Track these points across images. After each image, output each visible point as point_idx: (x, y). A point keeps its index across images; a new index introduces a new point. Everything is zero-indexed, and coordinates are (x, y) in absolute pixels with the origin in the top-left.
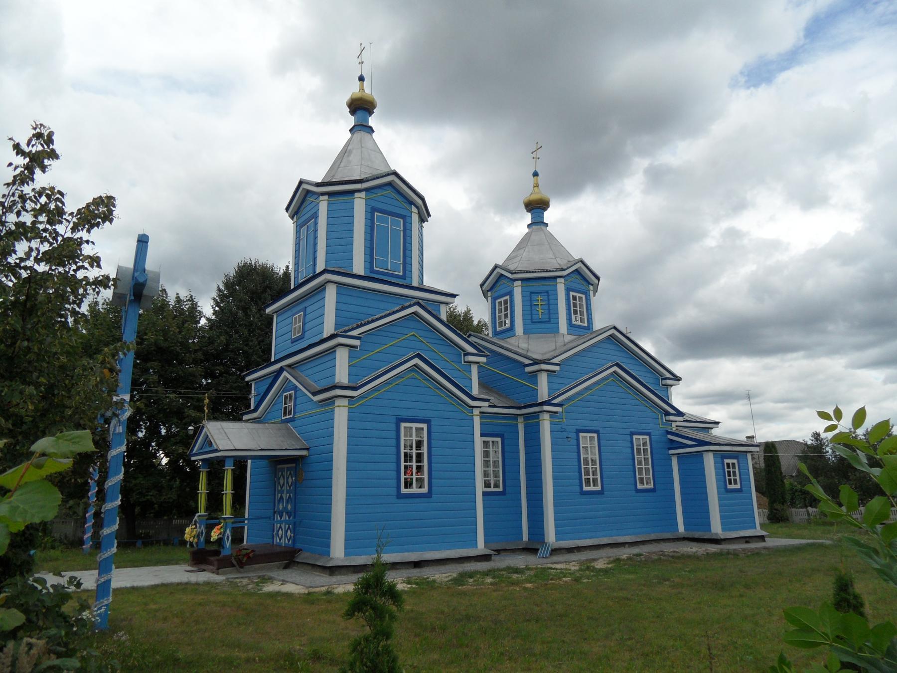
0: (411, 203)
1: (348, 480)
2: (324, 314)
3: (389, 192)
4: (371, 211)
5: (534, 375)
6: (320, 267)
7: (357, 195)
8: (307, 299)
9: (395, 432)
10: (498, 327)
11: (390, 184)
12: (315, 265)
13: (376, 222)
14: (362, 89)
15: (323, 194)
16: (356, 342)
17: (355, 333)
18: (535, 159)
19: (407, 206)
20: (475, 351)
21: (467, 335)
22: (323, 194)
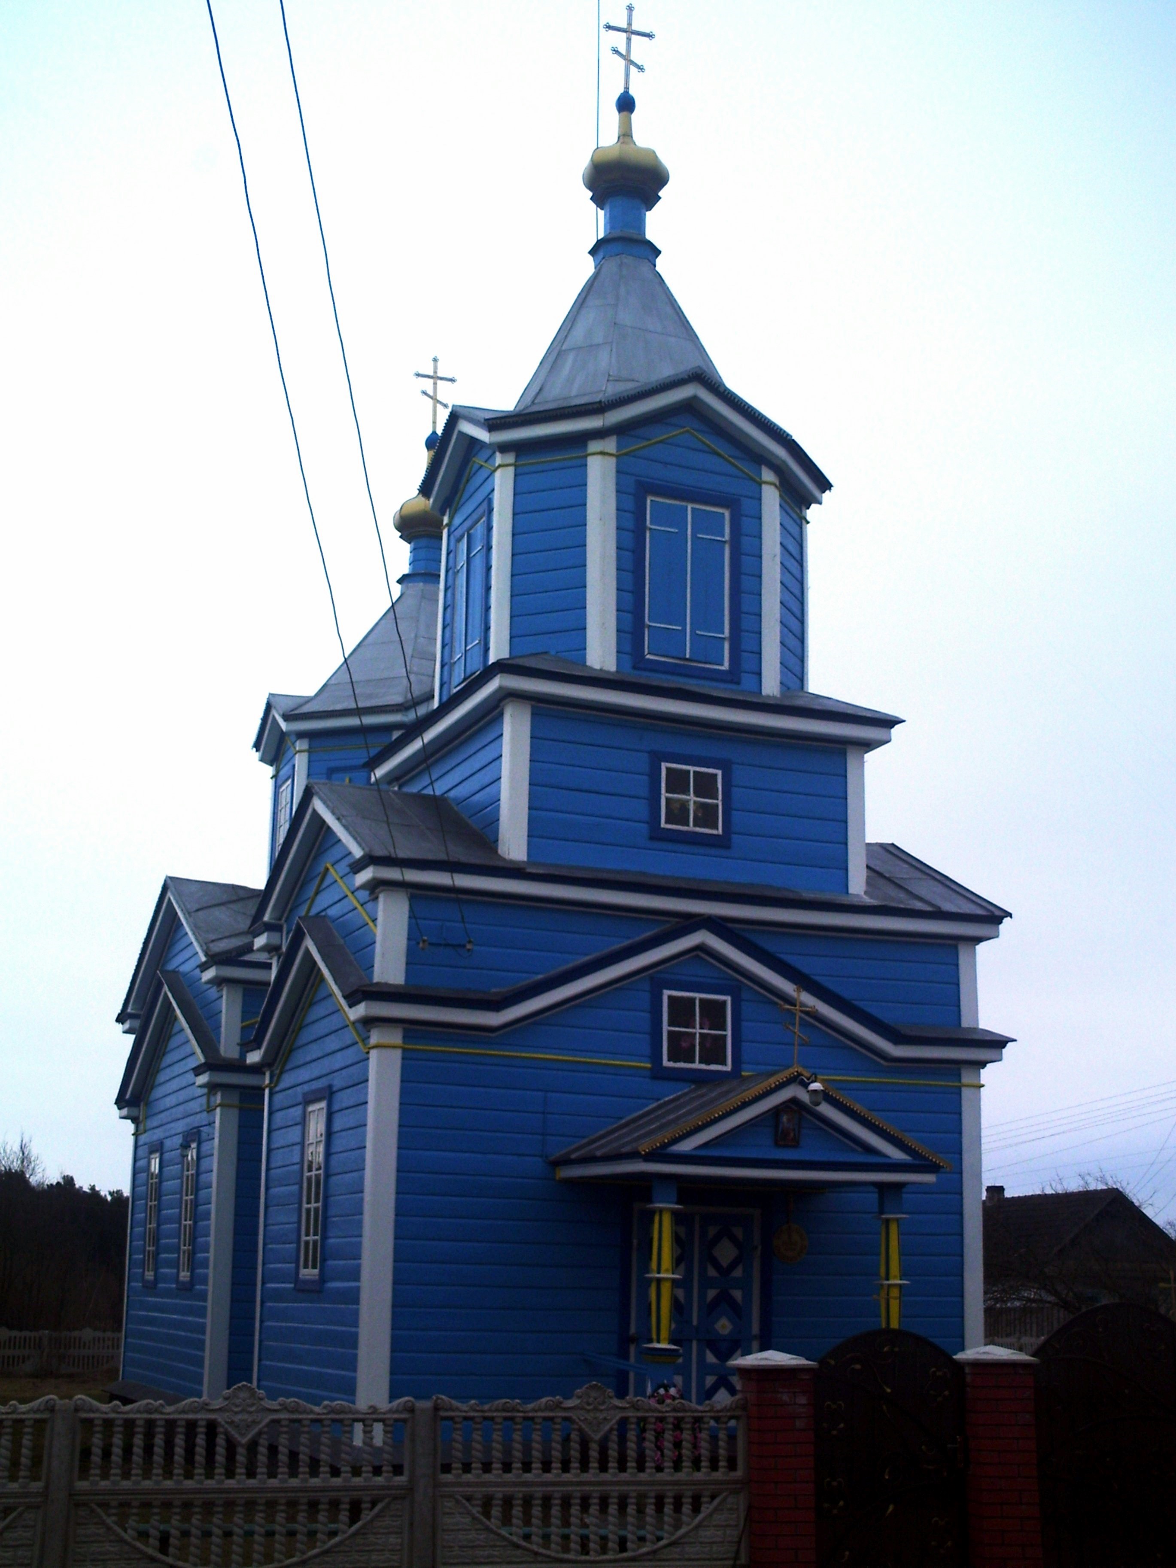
0: (761, 458)
2: (501, 756)
6: (498, 650)
9: (645, 826)
11: (690, 407)
12: (487, 649)
13: (651, 523)
14: (626, 134)
19: (746, 467)
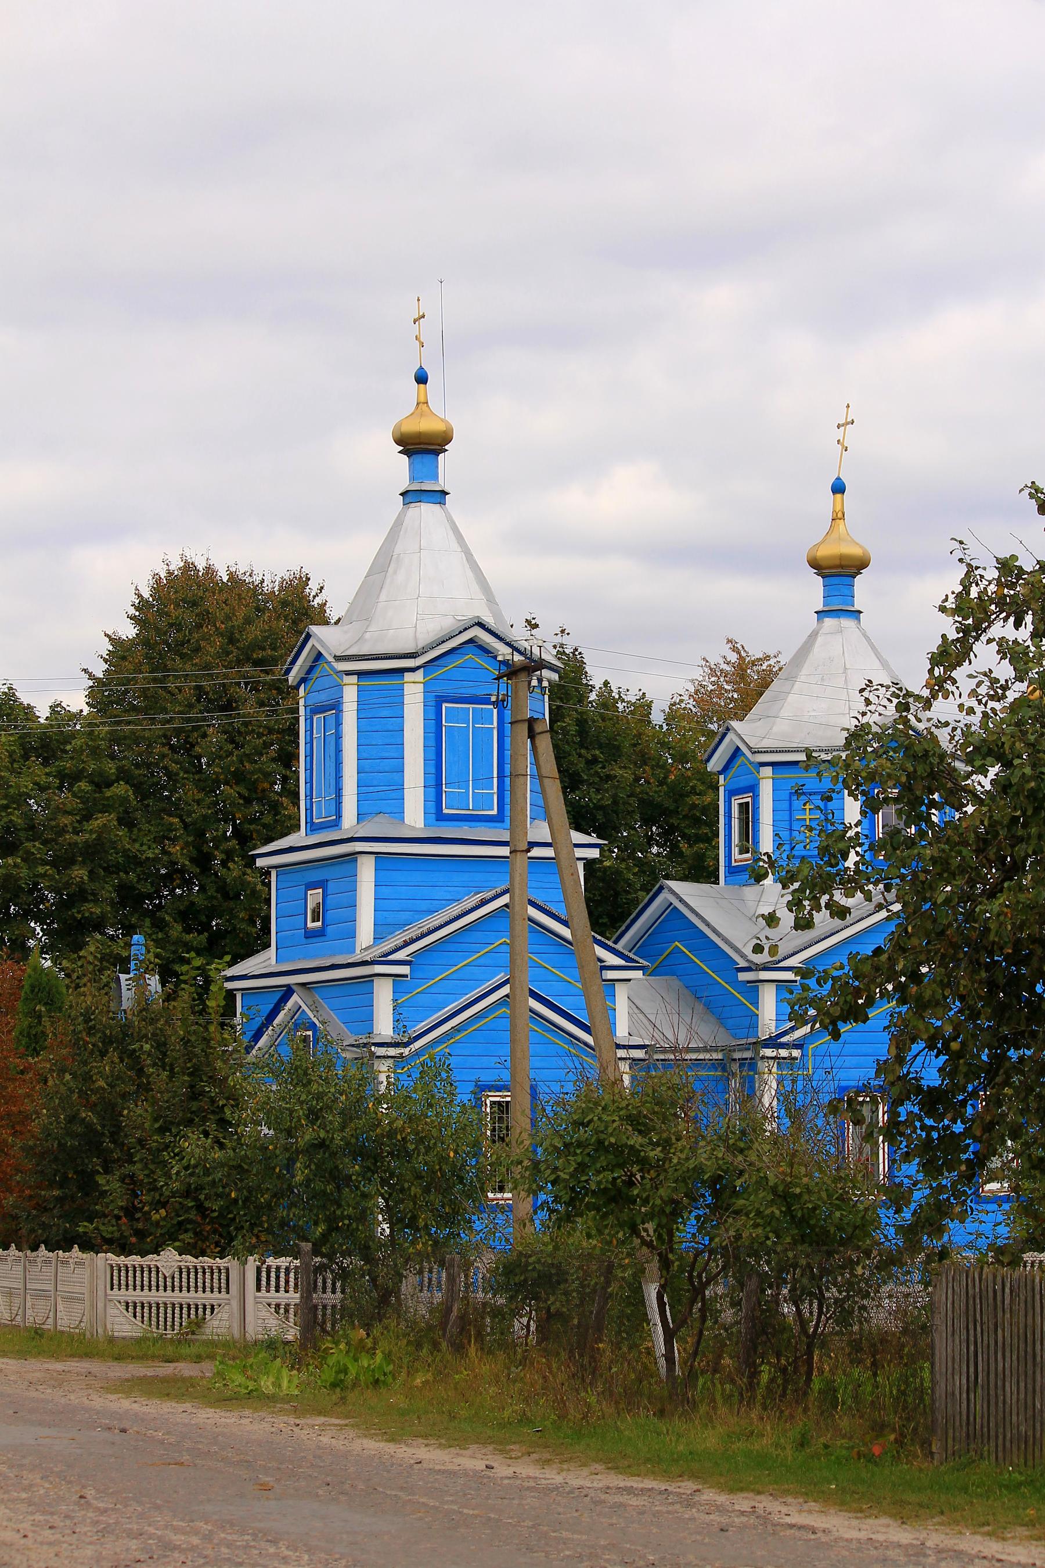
1: (397, 700)
3: (471, 657)
4: (435, 703)
5: (752, 989)
7: (408, 676)
8: (332, 865)
10: (735, 851)
15: (349, 673)
16: (405, 970)
17: (400, 955)
18: (842, 428)
20: (622, 962)
21: (613, 939)
22: (349, 673)
